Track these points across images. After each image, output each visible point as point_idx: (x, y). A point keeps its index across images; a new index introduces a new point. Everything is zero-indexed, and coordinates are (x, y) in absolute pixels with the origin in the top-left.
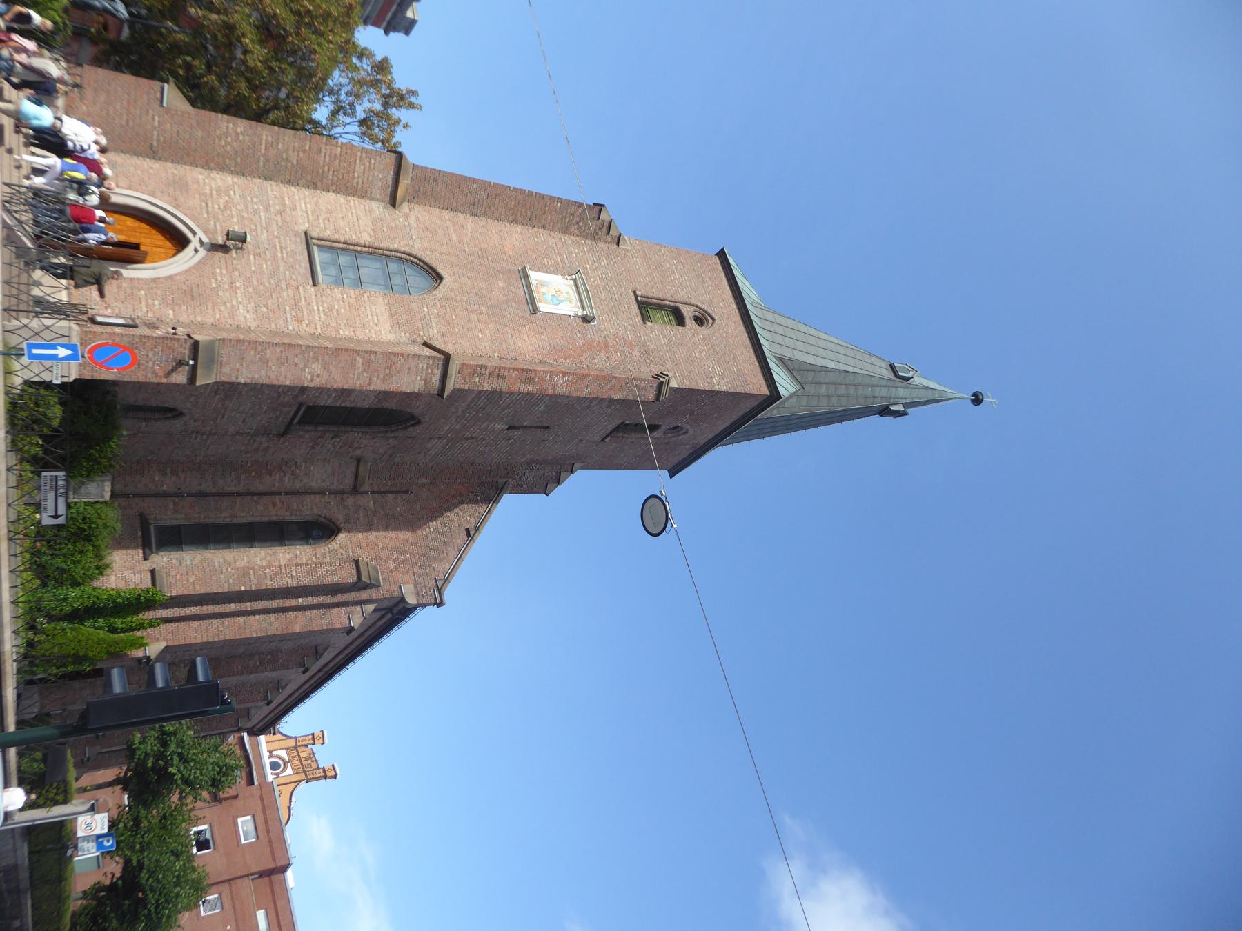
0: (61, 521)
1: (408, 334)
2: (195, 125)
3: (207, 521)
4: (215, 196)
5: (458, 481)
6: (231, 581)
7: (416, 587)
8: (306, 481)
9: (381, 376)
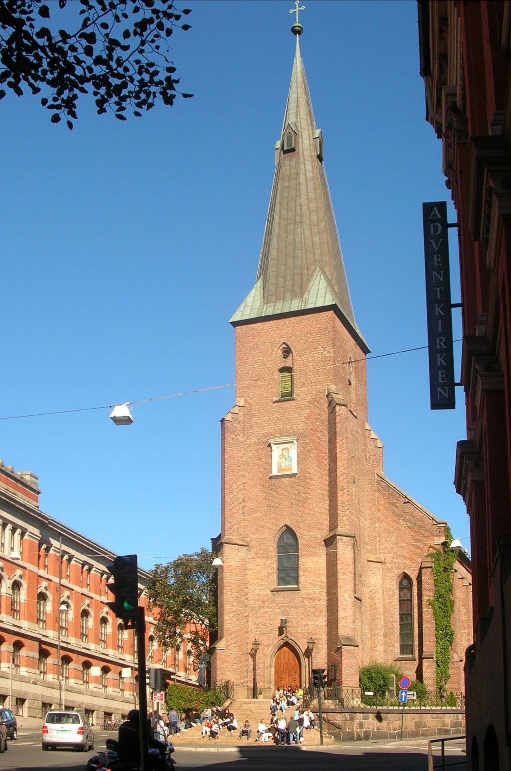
0: (415, 693)
1: (321, 548)
2: (230, 637)
3: (398, 633)
4: (261, 630)
5: (377, 504)
6: (429, 626)
7: (436, 536)
8: (378, 587)
9: (348, 566)
